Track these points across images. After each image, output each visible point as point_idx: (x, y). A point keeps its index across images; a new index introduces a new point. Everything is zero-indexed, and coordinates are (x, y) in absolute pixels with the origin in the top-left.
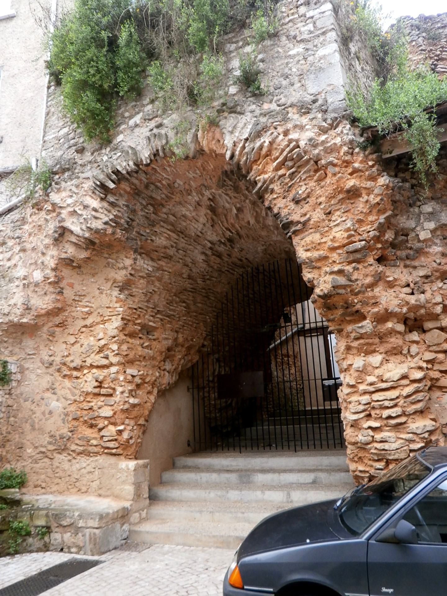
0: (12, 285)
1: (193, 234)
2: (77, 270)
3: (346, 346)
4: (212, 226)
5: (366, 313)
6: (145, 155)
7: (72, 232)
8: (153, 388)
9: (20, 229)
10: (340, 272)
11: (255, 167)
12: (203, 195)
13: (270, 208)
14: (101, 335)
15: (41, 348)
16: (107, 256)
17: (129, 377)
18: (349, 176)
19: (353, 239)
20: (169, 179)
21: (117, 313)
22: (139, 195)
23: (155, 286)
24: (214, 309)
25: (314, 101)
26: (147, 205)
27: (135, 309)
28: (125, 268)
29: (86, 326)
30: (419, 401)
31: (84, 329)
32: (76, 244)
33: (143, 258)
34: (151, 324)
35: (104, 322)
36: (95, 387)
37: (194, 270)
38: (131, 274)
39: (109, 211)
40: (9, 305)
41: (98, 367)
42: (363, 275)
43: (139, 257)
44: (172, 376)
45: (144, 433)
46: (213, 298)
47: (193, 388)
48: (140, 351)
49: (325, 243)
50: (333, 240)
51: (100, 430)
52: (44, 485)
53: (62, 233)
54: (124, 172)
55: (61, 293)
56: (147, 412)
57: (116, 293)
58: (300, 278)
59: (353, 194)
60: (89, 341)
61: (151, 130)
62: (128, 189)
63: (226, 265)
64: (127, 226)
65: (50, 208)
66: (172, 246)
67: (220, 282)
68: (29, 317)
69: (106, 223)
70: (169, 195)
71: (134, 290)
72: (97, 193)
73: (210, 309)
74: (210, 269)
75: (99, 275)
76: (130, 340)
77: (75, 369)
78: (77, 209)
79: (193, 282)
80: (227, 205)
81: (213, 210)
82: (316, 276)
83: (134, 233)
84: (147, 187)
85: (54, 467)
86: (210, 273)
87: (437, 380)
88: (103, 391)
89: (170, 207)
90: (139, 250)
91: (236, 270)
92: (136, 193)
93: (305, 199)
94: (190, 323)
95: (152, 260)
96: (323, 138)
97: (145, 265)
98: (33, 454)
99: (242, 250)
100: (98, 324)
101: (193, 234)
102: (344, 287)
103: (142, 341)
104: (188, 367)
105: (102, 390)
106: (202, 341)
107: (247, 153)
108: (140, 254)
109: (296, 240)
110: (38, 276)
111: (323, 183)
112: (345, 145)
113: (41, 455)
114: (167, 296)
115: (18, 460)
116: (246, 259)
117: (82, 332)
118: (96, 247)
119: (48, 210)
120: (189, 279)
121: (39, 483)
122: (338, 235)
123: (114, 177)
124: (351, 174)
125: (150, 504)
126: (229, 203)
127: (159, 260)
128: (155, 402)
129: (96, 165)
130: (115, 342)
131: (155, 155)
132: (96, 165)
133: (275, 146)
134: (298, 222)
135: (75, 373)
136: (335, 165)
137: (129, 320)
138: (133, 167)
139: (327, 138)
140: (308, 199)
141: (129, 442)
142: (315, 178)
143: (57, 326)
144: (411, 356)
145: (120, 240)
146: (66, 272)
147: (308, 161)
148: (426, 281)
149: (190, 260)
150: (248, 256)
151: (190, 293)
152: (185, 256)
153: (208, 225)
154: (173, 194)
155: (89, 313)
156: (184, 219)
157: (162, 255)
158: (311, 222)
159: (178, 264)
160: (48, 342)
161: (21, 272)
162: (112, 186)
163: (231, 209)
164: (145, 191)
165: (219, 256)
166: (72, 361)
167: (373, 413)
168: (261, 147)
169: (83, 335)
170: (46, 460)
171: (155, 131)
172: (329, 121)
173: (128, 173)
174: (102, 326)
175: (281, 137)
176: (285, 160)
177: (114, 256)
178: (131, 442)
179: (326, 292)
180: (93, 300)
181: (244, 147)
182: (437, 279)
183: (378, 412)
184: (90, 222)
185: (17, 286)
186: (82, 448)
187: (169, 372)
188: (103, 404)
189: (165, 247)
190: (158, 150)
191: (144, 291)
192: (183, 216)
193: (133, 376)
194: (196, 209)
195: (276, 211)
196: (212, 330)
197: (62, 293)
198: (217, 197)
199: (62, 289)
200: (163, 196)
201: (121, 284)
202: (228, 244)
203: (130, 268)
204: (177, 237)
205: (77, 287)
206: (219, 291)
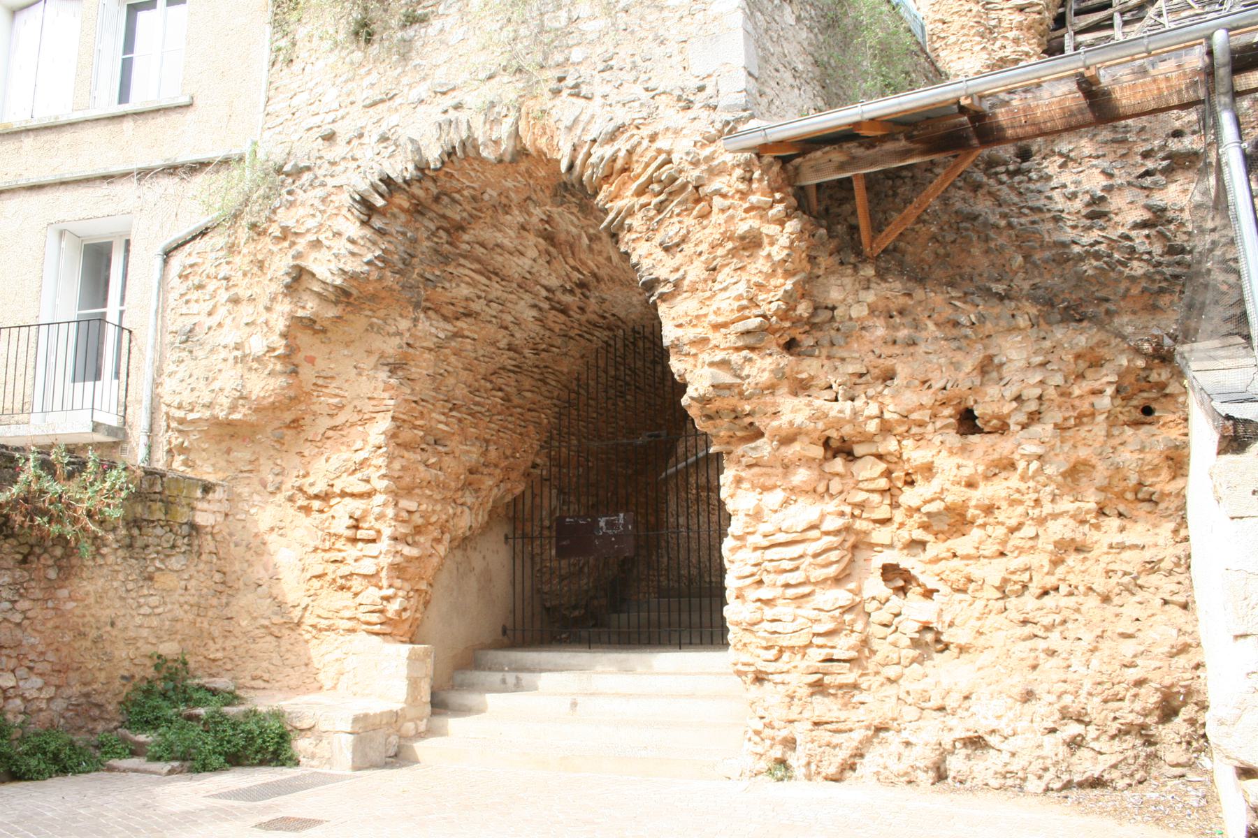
0: (215, 357)
1: (516, 276)
2: (322, 336)
3: (735, 476)
4: (548, 262)
5: (762, 428)
6: (433, 154)
7: (313, 275)
8: (443, 533)
9: (228, 263)
10: (724, 364)
11: (605, 187)
12: (529, 214)
13: (627, 255)
14: (359, 444)
15: (262, 461)
16: (369, 313)
17: (405, 515)
18: (744, 215)
19: (747, 312)
20: (473, 188)
21: (384, 408)
22: (422, 214)
23: (448, 364)
24: (555, 401)
25: (701, 89)
26: (438, 229)
27: (415, 402)
28: (399, 334)
29: (334, 428)
30: (832, 563)
31: (330, 433)
32: (319, 295)
33: (428, 318)
34: (441, 426)
35: (364, 422)
36: (348, 528)
37: (518, 335)
38: (408, 344)
39: (374, 243)
40: (213, 391)
41: (353, 495)
42: (762, 368)
43: (422, 316)
44: (477, 515)
45: (426, 604)
46: (553, 383)
47: (514, 538)
48: (423, 473)
49: (705, 315)
50: (717, 312)
51: (356, 594)
52: (266, 676)
53: (299, 275)
54: (400, 181)
55: (295, 372)
56: (430, 572)
57: (383, 375)
58: (667, 371)
59: (751, 243)
60: (340, 457)
61: (446, 112)
62: (406, 205)
63: (576, 325)
64: (401, 266)
65: (278, 234)
66: (479, 297)
67: (566, 354)
68: (245, 410)
69: (369, 263)
70: (474, 212)
71: (413, 370)
72: (356, 213)
73: (549, 401)
74: (548, 333)
75: (357, 344)
76: (406, 454)
77: (316, 497)
78: (322, 238)
79: (516, 355)
80: (574, 230)
81: (550, 238)
82: (689, 367)
83: (415, 276)
84: (437, 199)
85: (283, 649)
86: (547, 340)
87: (866, 533)
88: (361, 534)
89: (476, 232)
90: (424, 304)
91: (597, 333)
92: (418, 209)
93: (678, 245)
94: (510, 426)
95: (445, 318)
96: (707, 151)
97: (431, 328)
98: (250, 628)
99: (604, 301)
100: (353, 425)
101: (516, 276)
102: (729, 387)
103: (425, 455)
104: (507, 500)
105: (359, 532)
106: (531, 457)
107: (592, 164)
108: (426, 310)
109: (662, 309)
110: (257, 345)
111: (705, 222)
112: (738, 166)
113: (263, 630)
114: (470, 380)
115: (226, 637)
116: (613, 315)
117: (328, 438)
118: (351, 300)
119: (275, 237)
120: (509, 350)
121: (259, 673)
122: (725, 305)
123: (383, 187)
124: (747, 211)
125: (433, 714)
126: (576, 227)
127: (457, 319)
128: (446, 557)
129: (355, 164)
130: (381, 456)
131: (449, 155)
132: (355, 164)
133: (635, 158)
134: (667, 281)
135: (316, 504)
136: (724, 196)
137: (404, 421)
138: (415, 173)
139: (715, 152)
140: (683, 246)
141: (400, 616)
142: (695, 213)
143: (288, 427)
144: (832, 495)
145: (391, 289)
146: (304, 339)
147: (684, 187)
148: (859, 381)
149: (510, 318)
150: (615, 311)
151: (511, 375)
152: (501, 311)
153: (541, 261)
154: (480, 210)
155: (340, 407)
156: (499, 250)
157: (462, 310)
158: (686, 282)
159: (489, 326)
160: (273, 452)
161: (229, 336)
162: (379, 202)
163: (580, 237)
164: (434, 207)
165: (564, 311)
166: (312, 485)
167: (765, 578)
168: (614, 159)
169: (329, 442)
170: (269, 638)
171: (452, 114)
172: (718, 126)
173: (405, 181)
174: (360, 428)
175: (645, 143)
176: (650, 181)
177: (382, 313)
178: (405, 615)
179: (702, 393)
180: (346, 386)
181: (589, 155)
182: (877, 378)
183: (772, 576)
184: (343, 260)
185: (225, 360)
186: (327, 622)
187: (470, 509)
188: (360, 554)
189: (467, 299)
190: (454, 148)
191: (431, 372)
192: (498, 245)
193: (409, 512)
194: (519, 236)
195: (634, 259)
196: (551, 438)
197: (297, 373)
198: (556, 216)
199: (297, 366)
200: (465, 214)
201: (391, 361)
202: (578, 291)
203: (407, 335)
204: (487, 282)
205: (321, 363)
206: (566, 370)
